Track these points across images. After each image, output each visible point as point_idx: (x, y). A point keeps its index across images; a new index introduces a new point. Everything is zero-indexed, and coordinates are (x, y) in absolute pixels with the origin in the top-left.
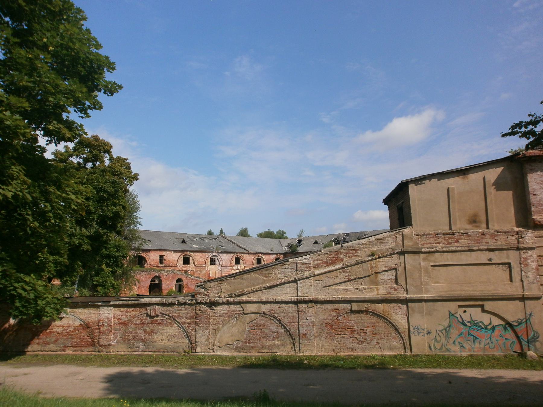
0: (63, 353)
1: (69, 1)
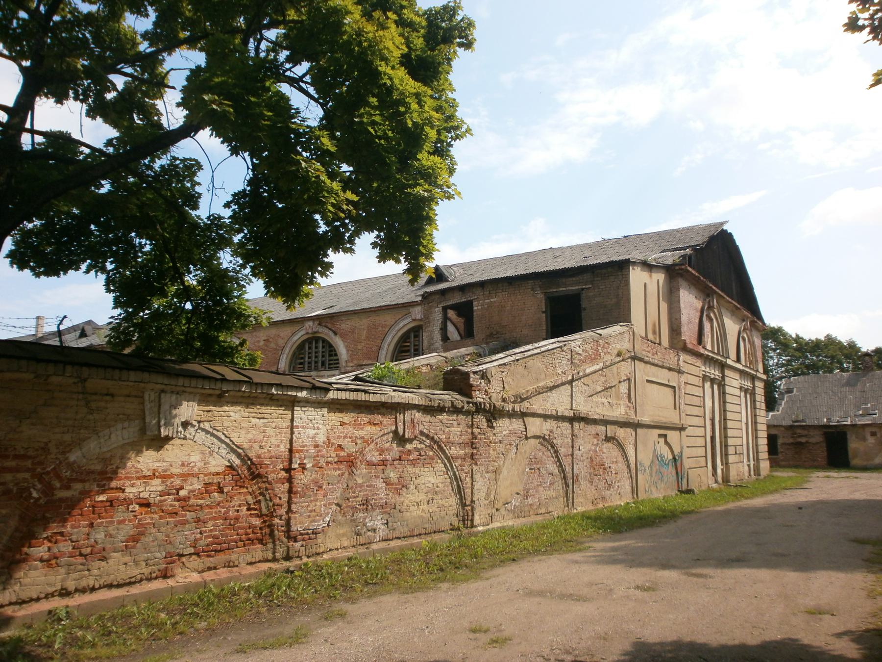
0: (157, 585)
1: (70, 3)
